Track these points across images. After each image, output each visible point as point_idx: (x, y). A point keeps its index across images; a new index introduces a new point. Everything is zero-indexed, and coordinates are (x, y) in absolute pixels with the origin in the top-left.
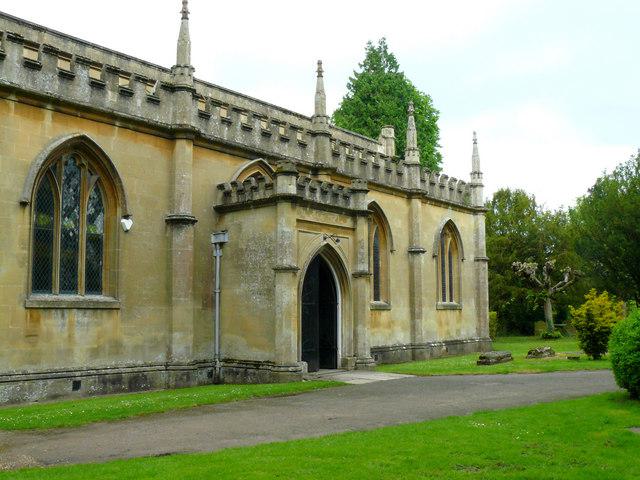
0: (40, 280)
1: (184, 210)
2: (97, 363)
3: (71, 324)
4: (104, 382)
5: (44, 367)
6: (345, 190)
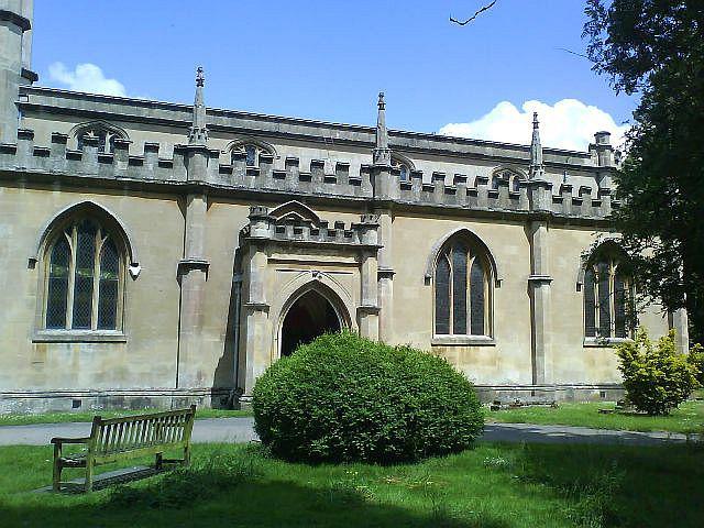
0: (55, 318)
1: (195, 256)
2: (102, 387)
3: (76, 354)
4: (105, 402)
5: (49, 388)
6: (347, 227)
